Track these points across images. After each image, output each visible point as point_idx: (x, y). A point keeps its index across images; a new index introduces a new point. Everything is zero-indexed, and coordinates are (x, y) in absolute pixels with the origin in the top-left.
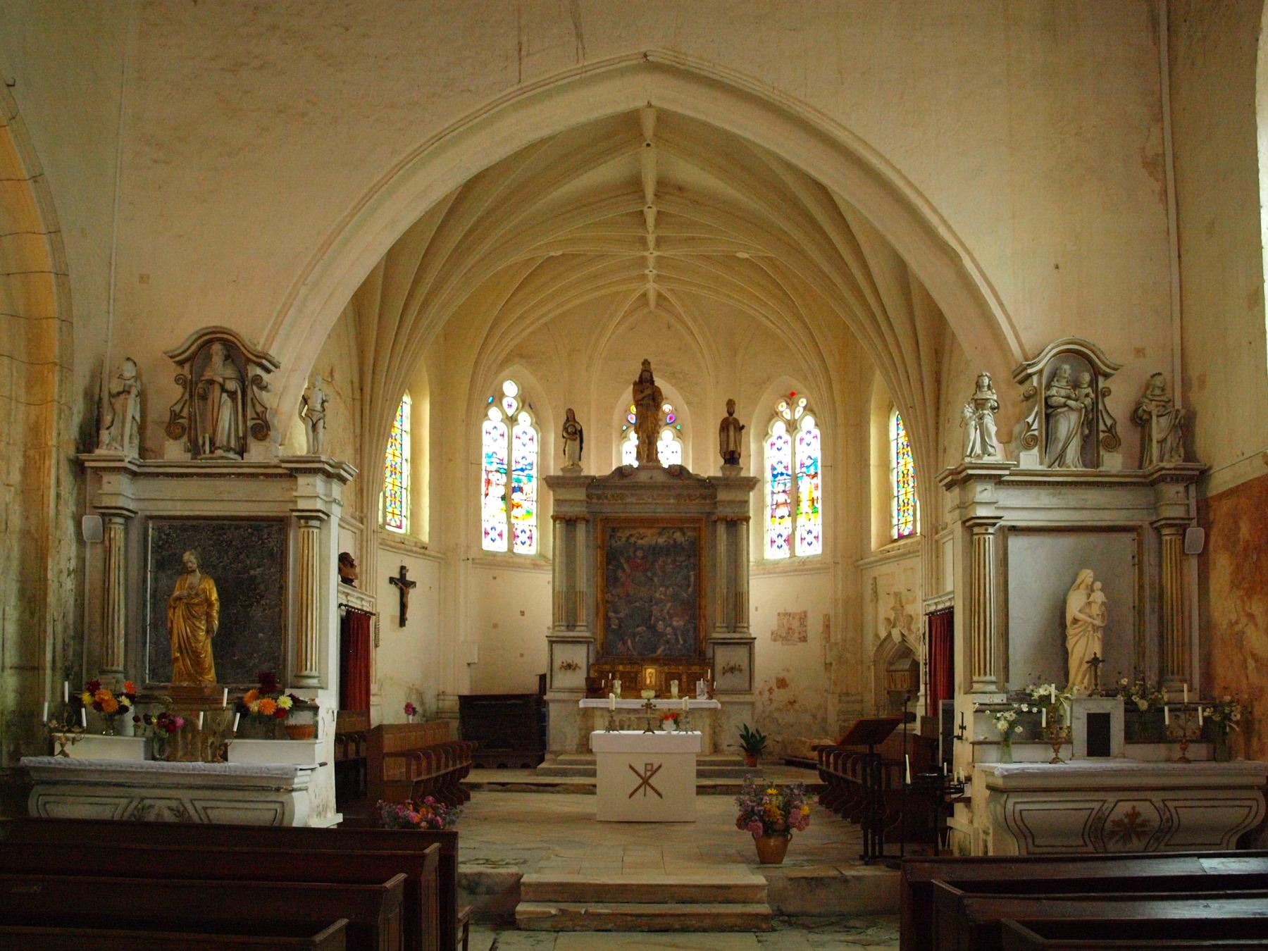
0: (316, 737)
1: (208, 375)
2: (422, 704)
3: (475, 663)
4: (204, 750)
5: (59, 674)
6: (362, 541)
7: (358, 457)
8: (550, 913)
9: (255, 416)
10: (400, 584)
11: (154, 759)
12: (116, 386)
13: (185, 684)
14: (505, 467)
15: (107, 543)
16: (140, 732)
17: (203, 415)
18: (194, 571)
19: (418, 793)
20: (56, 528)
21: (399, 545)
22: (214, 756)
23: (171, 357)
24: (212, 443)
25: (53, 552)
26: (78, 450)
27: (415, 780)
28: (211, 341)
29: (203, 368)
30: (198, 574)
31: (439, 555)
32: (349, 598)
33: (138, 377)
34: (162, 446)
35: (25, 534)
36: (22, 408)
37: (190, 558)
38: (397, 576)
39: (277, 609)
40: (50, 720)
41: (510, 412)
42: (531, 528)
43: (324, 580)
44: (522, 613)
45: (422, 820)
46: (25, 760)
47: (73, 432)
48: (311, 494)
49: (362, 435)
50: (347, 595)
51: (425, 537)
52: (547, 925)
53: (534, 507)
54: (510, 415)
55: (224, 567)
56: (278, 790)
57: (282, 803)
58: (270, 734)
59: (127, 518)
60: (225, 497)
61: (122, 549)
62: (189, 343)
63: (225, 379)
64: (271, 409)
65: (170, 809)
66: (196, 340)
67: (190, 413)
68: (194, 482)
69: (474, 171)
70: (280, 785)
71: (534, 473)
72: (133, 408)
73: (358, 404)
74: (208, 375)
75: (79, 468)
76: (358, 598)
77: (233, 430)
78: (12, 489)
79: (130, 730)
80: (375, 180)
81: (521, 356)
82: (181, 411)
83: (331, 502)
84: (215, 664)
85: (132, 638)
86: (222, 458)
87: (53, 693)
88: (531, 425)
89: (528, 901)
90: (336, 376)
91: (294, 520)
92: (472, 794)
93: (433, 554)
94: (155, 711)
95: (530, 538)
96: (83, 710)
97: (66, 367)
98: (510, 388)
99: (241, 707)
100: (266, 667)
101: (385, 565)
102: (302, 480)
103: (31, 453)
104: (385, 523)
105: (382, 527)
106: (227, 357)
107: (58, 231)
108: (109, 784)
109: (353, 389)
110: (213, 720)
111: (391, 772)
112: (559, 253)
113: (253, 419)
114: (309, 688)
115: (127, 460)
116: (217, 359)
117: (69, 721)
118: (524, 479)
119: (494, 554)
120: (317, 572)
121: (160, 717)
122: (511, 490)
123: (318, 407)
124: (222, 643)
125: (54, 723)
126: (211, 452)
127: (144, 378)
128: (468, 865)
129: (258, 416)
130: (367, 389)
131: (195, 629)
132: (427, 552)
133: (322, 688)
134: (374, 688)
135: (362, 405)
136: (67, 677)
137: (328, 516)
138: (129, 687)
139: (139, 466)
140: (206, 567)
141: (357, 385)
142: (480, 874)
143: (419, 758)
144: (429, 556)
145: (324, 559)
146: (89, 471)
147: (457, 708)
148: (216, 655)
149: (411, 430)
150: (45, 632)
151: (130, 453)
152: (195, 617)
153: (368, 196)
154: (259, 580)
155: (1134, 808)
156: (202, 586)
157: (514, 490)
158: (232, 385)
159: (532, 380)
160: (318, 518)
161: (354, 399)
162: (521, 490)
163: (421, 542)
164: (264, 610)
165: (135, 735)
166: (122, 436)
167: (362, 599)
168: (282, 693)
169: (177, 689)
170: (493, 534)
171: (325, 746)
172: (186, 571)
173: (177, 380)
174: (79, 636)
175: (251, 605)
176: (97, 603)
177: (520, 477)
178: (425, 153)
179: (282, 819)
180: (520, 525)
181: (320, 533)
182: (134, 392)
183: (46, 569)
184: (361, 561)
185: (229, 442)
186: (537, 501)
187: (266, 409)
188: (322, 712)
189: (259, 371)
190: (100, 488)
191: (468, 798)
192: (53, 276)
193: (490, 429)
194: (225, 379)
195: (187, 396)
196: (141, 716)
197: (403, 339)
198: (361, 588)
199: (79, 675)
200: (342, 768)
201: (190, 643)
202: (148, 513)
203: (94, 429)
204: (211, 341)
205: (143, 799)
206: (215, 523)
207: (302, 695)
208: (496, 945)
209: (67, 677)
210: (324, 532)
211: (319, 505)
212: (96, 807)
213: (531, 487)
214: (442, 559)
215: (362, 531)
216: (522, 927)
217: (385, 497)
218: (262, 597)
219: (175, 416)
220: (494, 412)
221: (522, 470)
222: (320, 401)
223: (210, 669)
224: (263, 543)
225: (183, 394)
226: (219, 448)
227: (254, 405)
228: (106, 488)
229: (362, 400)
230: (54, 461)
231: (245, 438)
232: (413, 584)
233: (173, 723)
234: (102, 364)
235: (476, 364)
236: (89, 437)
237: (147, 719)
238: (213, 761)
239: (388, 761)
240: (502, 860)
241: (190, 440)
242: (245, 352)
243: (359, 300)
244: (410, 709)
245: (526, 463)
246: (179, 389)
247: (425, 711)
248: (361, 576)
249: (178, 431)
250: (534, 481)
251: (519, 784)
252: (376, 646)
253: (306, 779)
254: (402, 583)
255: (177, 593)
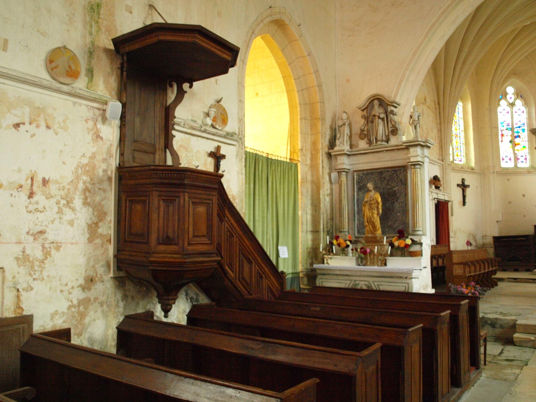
0: (422, 256)
1: (373, 113)
2: (475, 241)
3: (500, 221)
4: (377, 262)
5: (326, 233)
6: (443, 169)
7: (439, 133)
8: (531, 339)
9: (392, 126)
10: (462, 187)
11: (359, 265)
12: (340, 123)
13: (370, 235)
14: (511, 127)
15: (340, 182)
16: (354, 255)
17: (372, 129)
18: (371, 191)
19: (468, 281)
20: (323, 178)
21: (461, 169)
22: (381, 264)
23: (359, 109)
24: (376, 139)
25: (322, 187)
26: (329, 149)
27: (467, 275)
28: (374, 100)
29: (371, 111)
30: (373, 191)
31: (480, 172)
32: (438, 195)
33: (348, 118)
34: (358, 143)
35: (313, 182)
36: (310, 136)
37: (370, 186)
38: (460, 183)
39: (404, 203)
40: (323, 250)
41: (511, 101)
42: (526, 154)
43: (423, 190)
44: (524, 196)
45: (469, 293)
46: (315, 266)
47: (326, 142)
48: (416, 154)
49: (440, 123)
50: (437, 194)
51: (473, 164)
52: (529, 344)
53: (527, 144)
54: (511, 103)
55: (383, 188)
56: (406, 278)
57: (408, 283)
58: (403, 255)
59: (347, 172)
60: (383, 160)
61: (346, 185)
62: (365, 102)
63: (379, 114)
64: (398, 122)
65: (365, 285)
66: (368, 100)
67: (367, 129)
68: (370, 156)
69: (476, 5)
70: (406, 276)
71: (526, 127)
72: (347, 130)
73: (438, 111)
74: (373, 113)
75: (329, 155)
76: (442, 195)
77: (384, 133)
78: (308, 166)
79: (351, 254)
80: (434, 20)
81: (515, 74)
82: (364, 128)
83: (424, 157)
84: (381, 227)
85: (350, 217)
86: (380, 145)
87: (324, 241)
88: (522, 105)
89: (520, 333)
90: (427, 100)
91: (409, 166)
92: (499, 283)
93: (478, 171)
94: (359, 246)
95: (526, 159)
96: (334, 247)
97: (323, 119)
98: (510, 90)
99: (391, 244)
100: (401, 227)
101: (455, 179)
102: (412, 150)
103: (313, 152)
104: (454, 160)
105: (453, 162)
106: (380, 105)
107: (318, 71)
108: (343, 275)
109: (435, 104)
110: (381, 249)
111: (457, 272)
112: (529, 23)
113: (391, 127)
114: (418, 235)
115: (346, 150)
116: (376, 107)
117: (329, 251)
118: (521, 132)
119: (507, 169)
120: (419, 186)
121: (361, 249)
122: (514, 137)
123: (417, 119)
124: (384, 218)
125: (324, 252)
126: (376, 143)
127: (350, 118)
128: (492, 314)
129: (393, 126)
130: (441, 103)
131: (373, 213)
132: (474, 171)
133: (424, 235)
134: (451, 234)
135: (439, 111)
136: (328, 234)
137: (423, 163)
138: (350, 237)
139: (350, 152)
140: (376, 188)
141: (436, 102)
142: (497, 319)
143: (469, 266)
144: (475, 173)
145: (422, 181)
146: (333, 157)
147: (492, 242)
148: (381, 223)
149: (464, 117)
150: (320, 218)
151: (346, 148)
152: (373, 209)
153: (431, 28)
154: (397, 192)
155: (218, 148)
156: (375, 196)
157: (516, 137)
158: (382, 116)
159: (520, 83)
160: (419, 164)
161: (436, 109)
162: (519, 136)
163: (471, 167)
164: (399, 204)
165: (353, 256)
166: (344, 141)
167: (444, 195)
168: (407, 237)
169: (367, 238)
170: (507, 159)
171: (426, 260)
172: (369, 191)
173: (362, 117)
174: (332, 219)
175: (394, 202)
176: (338, 206)
177: (519, 131)
178: (453, 4)
179: (408, 290)
180: (519, 154)
181: (420, 170)
182: (347, 124)
183: (319, 194)
184: (443, 178)
185: (382, 138)
186: (528, 141)
187: (396, 122)
188: (424, 245)
189: (392, 108)
190: (337, 162)
191: (497, 285)
192: (317, 87)
193: (501, 111)
194: (379, 114)
195: (366, 123)
196: (354, 249)
197: (455, 79)
198: (444, 190)
199: (332, 233)
200: (434, 270)
201: (371, 219)
202: (354, 169)
203: (334, 140)
204: (374, 100)
205: (355, 281)
206: (379, 170)
207: (416, 239)
208: (503, 351)
209: (328, 234)
210: (422, 170)
211: (419, 159)
212: (339, 284)
213: (525, 135)
214: (481, 173)
215: (443, 165)
216: (517, 344)
217: (453, 149)
218: (398, 199)
219: (362, 131)
220: (503, 103)
221: (519, 127)
222: (417, 116)
223: (379, 229)
224: (398, 177)
225: (364, 123)
226: (379, 141)
227: (391, 122)
228: (339, 162)
229: (439, 108)
230: (321, 154)
231: (388, 136)
232: (468, 186)
233: (366, 251)
234: (335, 116)
235: (492, 82)
236: (332, 144)
237: (356, 250)
238: (381, 266)
239: (456, 267)
240: (509, 313)
241: (368, 139)
242: (387, 102)
243: (435, 66)
244: (469, 243)
245: (521, 123)
246: (363, 120)
247: (477, 244)
248: (444, 185)
249: (364, 136)
250: (526, 131)
251: (523, 279)
252: (452, 215)
253: (417, 274)
254: (463, 186)
255: (366, 200)
